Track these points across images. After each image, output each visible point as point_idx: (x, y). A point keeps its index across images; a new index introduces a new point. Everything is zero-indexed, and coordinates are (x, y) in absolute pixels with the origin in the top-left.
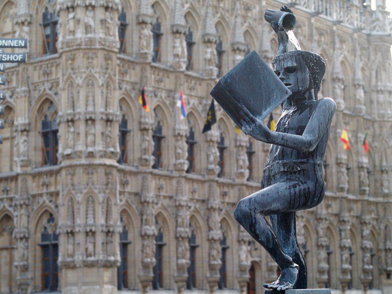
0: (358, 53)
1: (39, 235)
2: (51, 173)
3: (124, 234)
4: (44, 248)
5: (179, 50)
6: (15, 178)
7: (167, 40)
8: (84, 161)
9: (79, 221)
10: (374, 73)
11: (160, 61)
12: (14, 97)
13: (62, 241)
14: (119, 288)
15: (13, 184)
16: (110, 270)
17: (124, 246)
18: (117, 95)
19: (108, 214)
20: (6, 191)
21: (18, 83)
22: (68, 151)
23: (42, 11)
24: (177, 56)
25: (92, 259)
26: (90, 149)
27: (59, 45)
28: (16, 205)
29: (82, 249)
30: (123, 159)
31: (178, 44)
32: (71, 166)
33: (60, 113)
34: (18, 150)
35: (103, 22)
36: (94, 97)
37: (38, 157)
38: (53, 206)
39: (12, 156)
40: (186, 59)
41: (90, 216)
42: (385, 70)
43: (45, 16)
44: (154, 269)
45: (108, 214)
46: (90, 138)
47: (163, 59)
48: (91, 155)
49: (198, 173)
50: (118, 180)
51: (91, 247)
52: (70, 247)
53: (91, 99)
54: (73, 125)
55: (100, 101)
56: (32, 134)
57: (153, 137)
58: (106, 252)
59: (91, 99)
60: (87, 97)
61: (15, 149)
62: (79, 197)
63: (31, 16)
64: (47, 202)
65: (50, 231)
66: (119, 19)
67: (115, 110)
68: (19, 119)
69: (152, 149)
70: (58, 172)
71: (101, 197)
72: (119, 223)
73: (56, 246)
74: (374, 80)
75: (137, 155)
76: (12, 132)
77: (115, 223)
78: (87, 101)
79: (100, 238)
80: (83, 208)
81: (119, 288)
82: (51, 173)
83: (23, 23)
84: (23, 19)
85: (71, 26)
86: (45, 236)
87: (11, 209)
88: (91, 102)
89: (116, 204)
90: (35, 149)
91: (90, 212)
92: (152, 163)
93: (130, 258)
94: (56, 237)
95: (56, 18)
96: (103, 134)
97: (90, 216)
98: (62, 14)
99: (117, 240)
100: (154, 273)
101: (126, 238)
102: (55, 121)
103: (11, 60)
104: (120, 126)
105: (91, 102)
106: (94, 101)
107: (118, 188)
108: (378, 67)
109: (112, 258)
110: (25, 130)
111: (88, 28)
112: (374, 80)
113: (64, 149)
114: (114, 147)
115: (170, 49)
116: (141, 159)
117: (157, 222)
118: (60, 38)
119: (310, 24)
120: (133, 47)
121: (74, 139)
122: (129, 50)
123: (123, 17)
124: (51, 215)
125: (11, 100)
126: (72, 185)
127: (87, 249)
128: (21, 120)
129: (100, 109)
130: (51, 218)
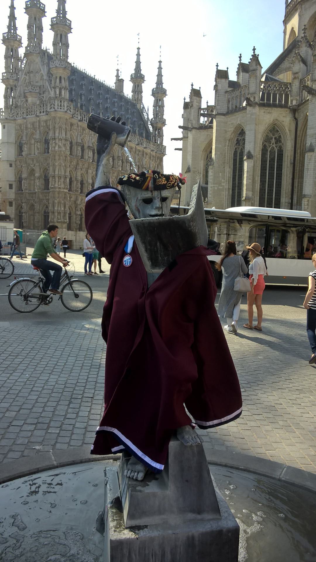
0: (152, 158)
1: (43, 212)
2: (46, 193)
3: (70, 214)
4: (45, 216)
5: (90, 155)
6: (35, 193)
7: (86, 151)
8: (57, 190)
9: (56, 208)
10: (156, 166)
11: (83, 158)
12: (35, 166)
13: (50, 214)
14: (68, 230)
15: (35, 195)
16: (65, 224)
17: (70, 218)
18: (68, 170)
19: (65, 207)
20: (32, 197)
21: (36, 162)
22: (53, 186)
23: (44, 138)
24: (89, 157)
25: (60, 220)
26: (59, 186)
27: (50, 151)
28: (36, 202)
29: (56, 217)
30: (70, 190)
31: (90, 153)
32: (53, 191)
33: (50, 174)
34: (36, 184)
35: (65, 145)
36: (61, 170)
37: (43, 187)
38: (47, 203)
39: (34, 185)
40: (92, 158)
41: (59, 207)
42: (160, 165)
43: (45, 139)
44: (79, 225)
45: (65, 207)
46: (60, 183)
47: (85, 157)
48: (60, 188)
49: (32, 228)
50: (68, 197)
51: (59, 217)
52: (53, 216)
53: (60, 170)
54: (55, 140)
55: (63, 171)
56: (41, 179)
57: (80, 183)
58: (64, 218)
59: (60, 170)
60: (59, 169)
61: (35, 184)
62: (56, 201)
63: (40, 139)
64: (46, 201)
65: (47, 211)
66: (70, 143)
67: (68, 174)
68: (37, 174)
69: (79, 187)
70: (49, 192)
71: (63, 202)
72: (68, 210)
73: (48, 216)
74: (156, 168)
75: (75, 189)
76: (34, 178)
77: (67, 210)
78: (59, 171)
79: (62, 215)
80: (57, 205)
81: (68, 230)
82: (46, 193)
83: (38, 142)
84: (38, 140)
85: (54, 145)
86: (45, 212)
87: (34, 203)
88: (60, 171)
89: (67, 204)
90: (42, 184)
91: (59, 205)
92: (80, 192)
93: (72, 221)
94: (48, 213)
95: (49, 141)
96: (64, 182)
97: (59, 207)
98: (51, 141)
99: (67, 215)
100: (79, 226)
101: (71, 215)
102: (48, 176)
103: (134, 478)
104: (69, 179)
105: (60, 171)
106: (61, 171)
107: (68, 199)
108: (158, 164)
109: (66, 221)
110: (38, 178)
111: (59, 147)
112: (156, 168)
113: (51, 186)
114: (67, 186)
115: (87, 154)
116: (76, 190)
117: (81, 210)
118: (50, 149)
119: (136, 148)
120: (74, 153)
121: (54, 183)
122: (73, 154)
123: (71, 143)
124: (47, 206)
125: (34, 168)
126: (54, 197)
127: (58, 218)
128: (37, 175)
129: (63, 173)
130: (47, 207)
